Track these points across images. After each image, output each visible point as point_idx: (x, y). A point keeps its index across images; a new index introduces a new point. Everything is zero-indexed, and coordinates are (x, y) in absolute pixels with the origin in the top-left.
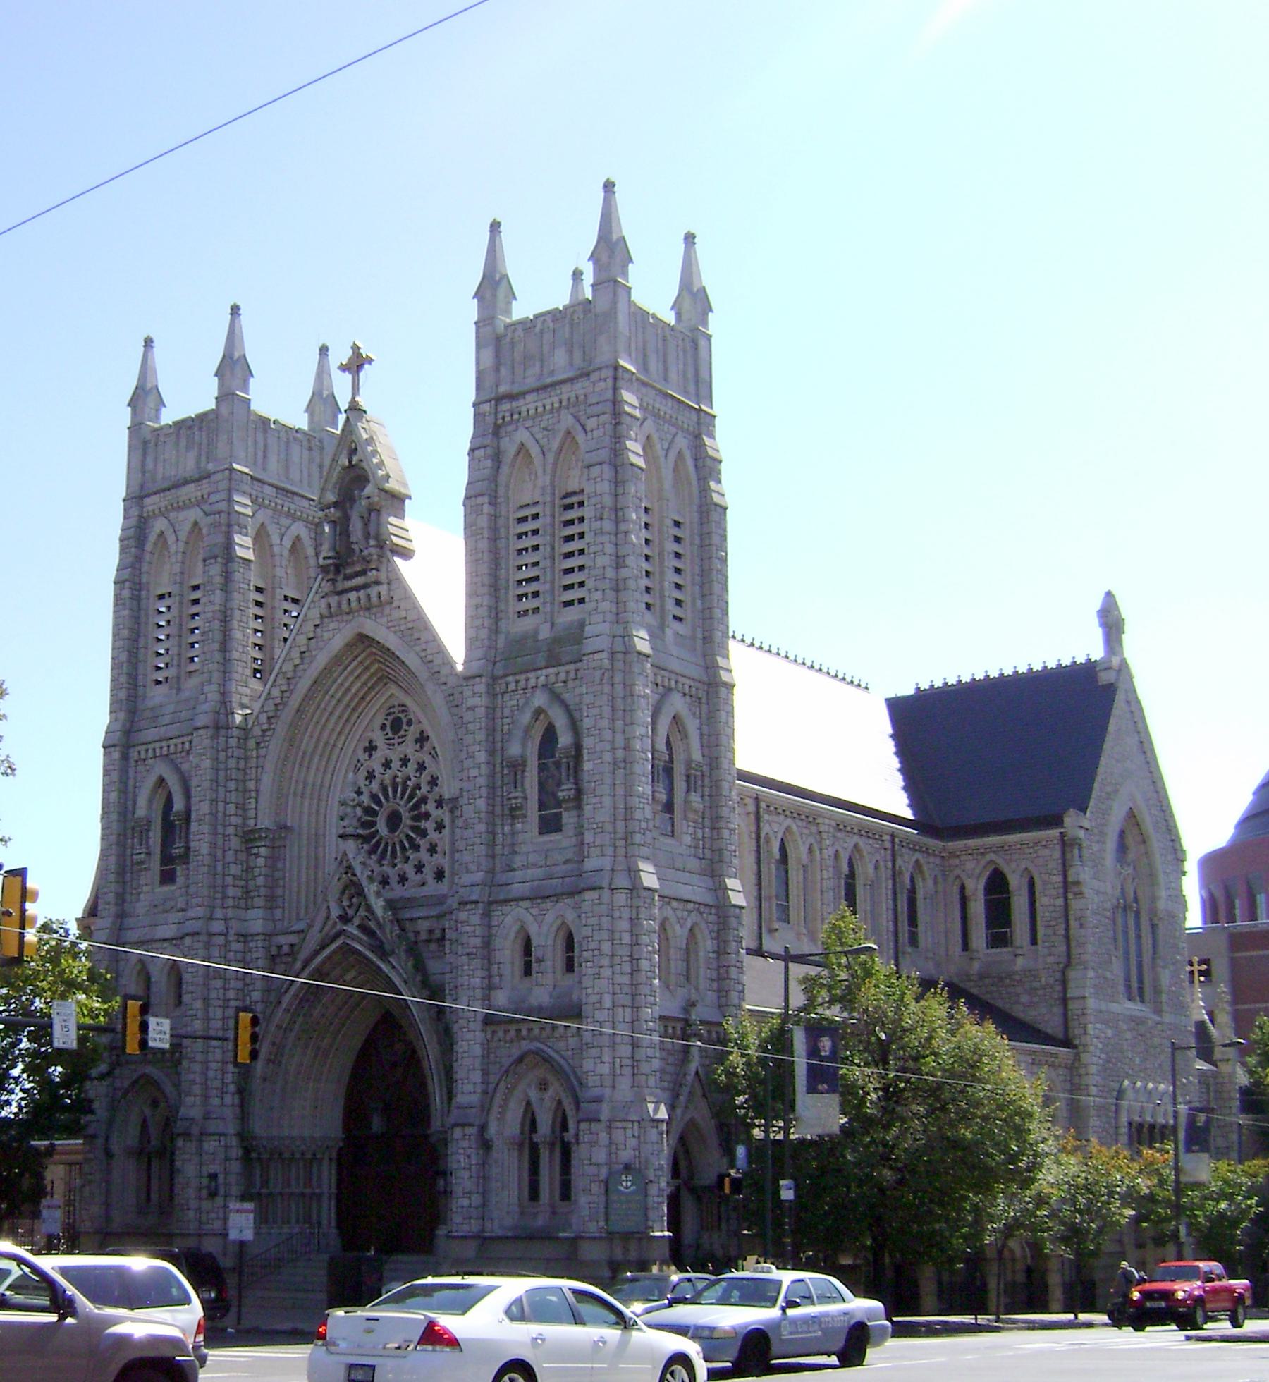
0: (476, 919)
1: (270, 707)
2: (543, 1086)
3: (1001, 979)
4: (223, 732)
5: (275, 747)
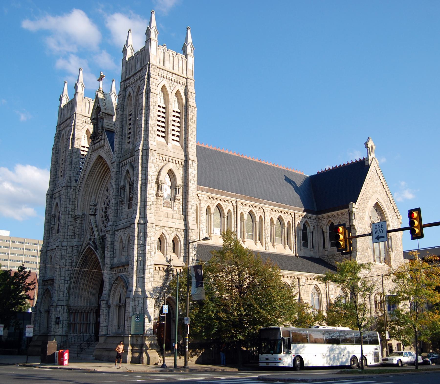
0: (109, 236)
3: (333, 256)
4: (69, 188)
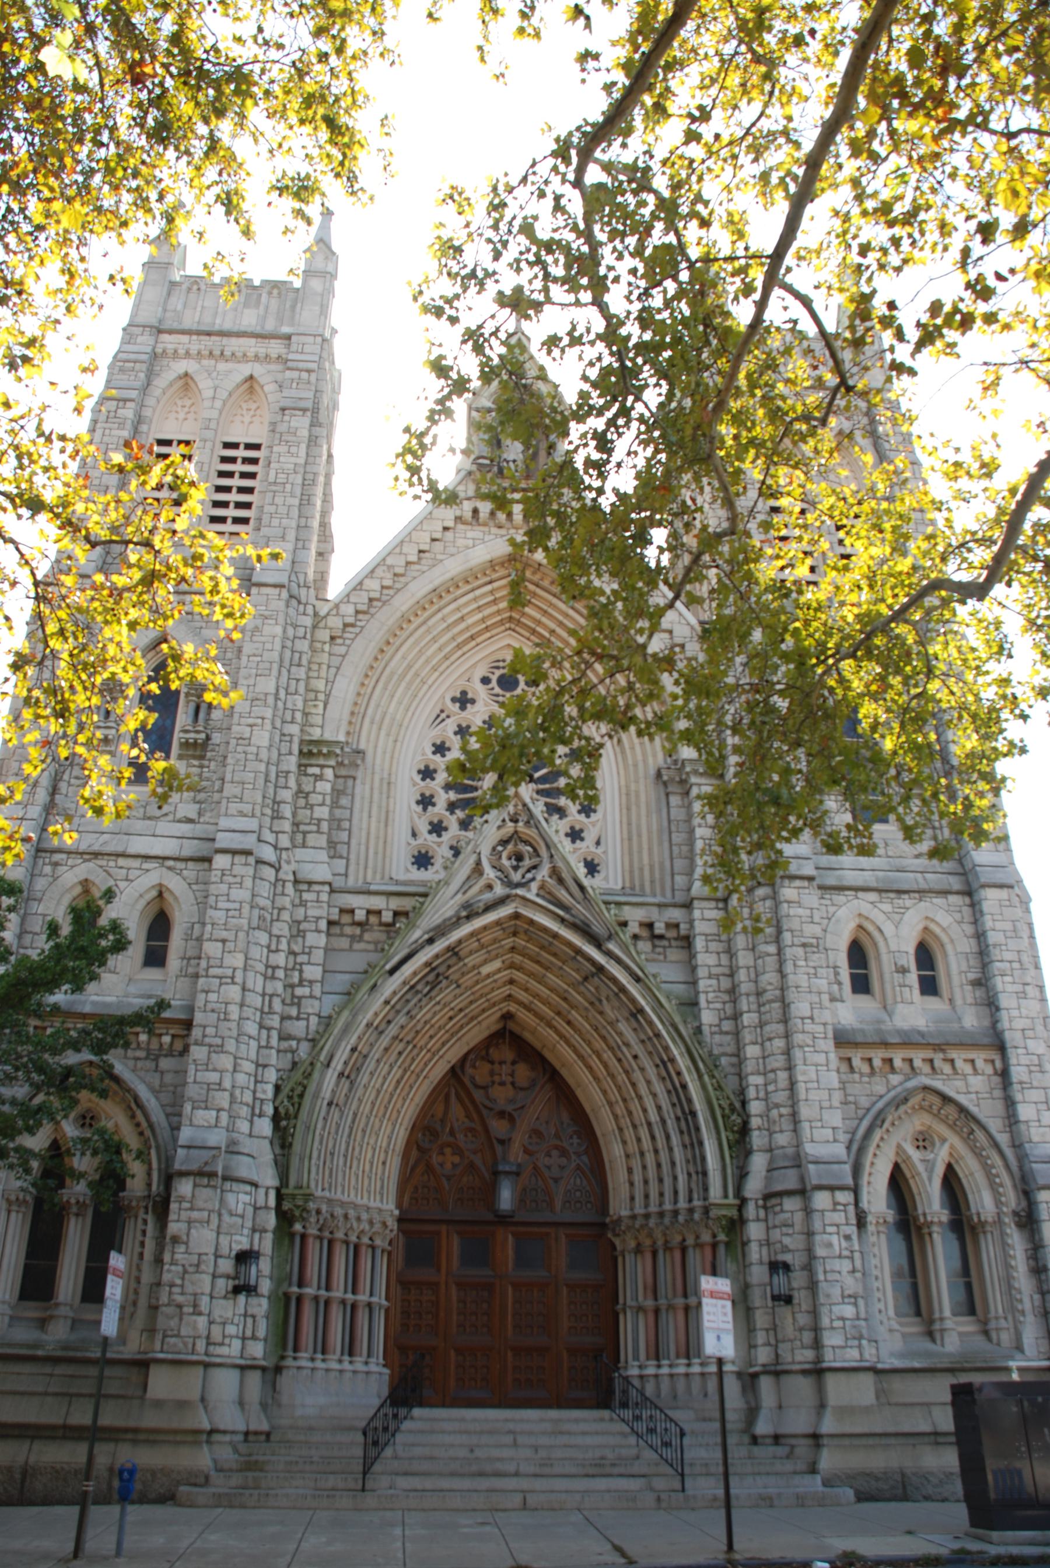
1: (363, 598)
2: (923, 1141)
5: (362, 649)
